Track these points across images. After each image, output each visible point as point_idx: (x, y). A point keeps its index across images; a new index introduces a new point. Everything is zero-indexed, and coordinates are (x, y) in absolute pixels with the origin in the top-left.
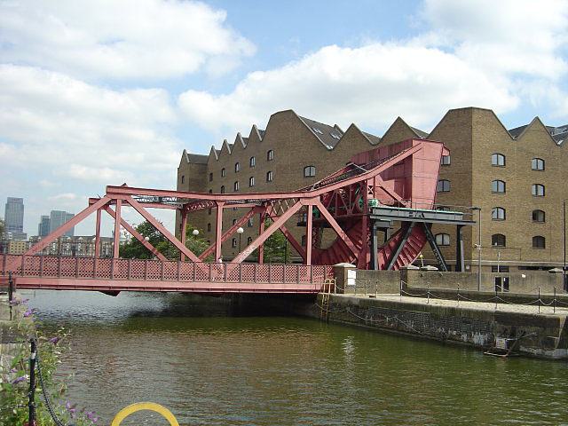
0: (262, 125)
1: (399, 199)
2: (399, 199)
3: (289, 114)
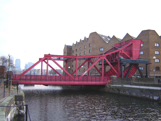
0: (88, 37)
1: (129, 56)
2: (129, 56)
3: (95, 33)
